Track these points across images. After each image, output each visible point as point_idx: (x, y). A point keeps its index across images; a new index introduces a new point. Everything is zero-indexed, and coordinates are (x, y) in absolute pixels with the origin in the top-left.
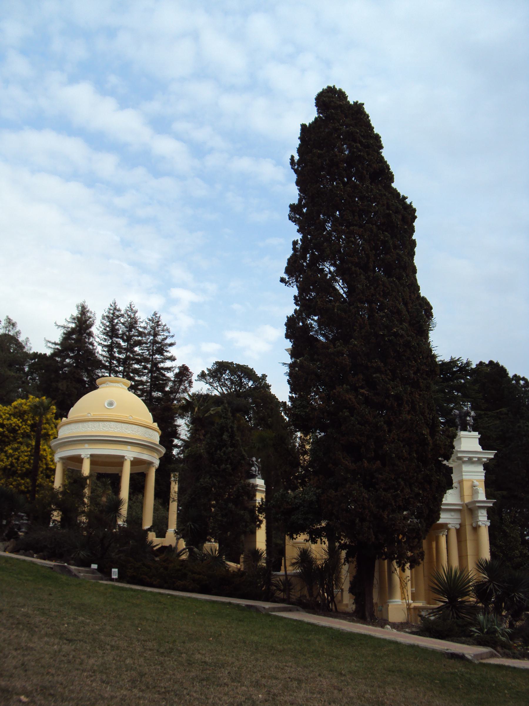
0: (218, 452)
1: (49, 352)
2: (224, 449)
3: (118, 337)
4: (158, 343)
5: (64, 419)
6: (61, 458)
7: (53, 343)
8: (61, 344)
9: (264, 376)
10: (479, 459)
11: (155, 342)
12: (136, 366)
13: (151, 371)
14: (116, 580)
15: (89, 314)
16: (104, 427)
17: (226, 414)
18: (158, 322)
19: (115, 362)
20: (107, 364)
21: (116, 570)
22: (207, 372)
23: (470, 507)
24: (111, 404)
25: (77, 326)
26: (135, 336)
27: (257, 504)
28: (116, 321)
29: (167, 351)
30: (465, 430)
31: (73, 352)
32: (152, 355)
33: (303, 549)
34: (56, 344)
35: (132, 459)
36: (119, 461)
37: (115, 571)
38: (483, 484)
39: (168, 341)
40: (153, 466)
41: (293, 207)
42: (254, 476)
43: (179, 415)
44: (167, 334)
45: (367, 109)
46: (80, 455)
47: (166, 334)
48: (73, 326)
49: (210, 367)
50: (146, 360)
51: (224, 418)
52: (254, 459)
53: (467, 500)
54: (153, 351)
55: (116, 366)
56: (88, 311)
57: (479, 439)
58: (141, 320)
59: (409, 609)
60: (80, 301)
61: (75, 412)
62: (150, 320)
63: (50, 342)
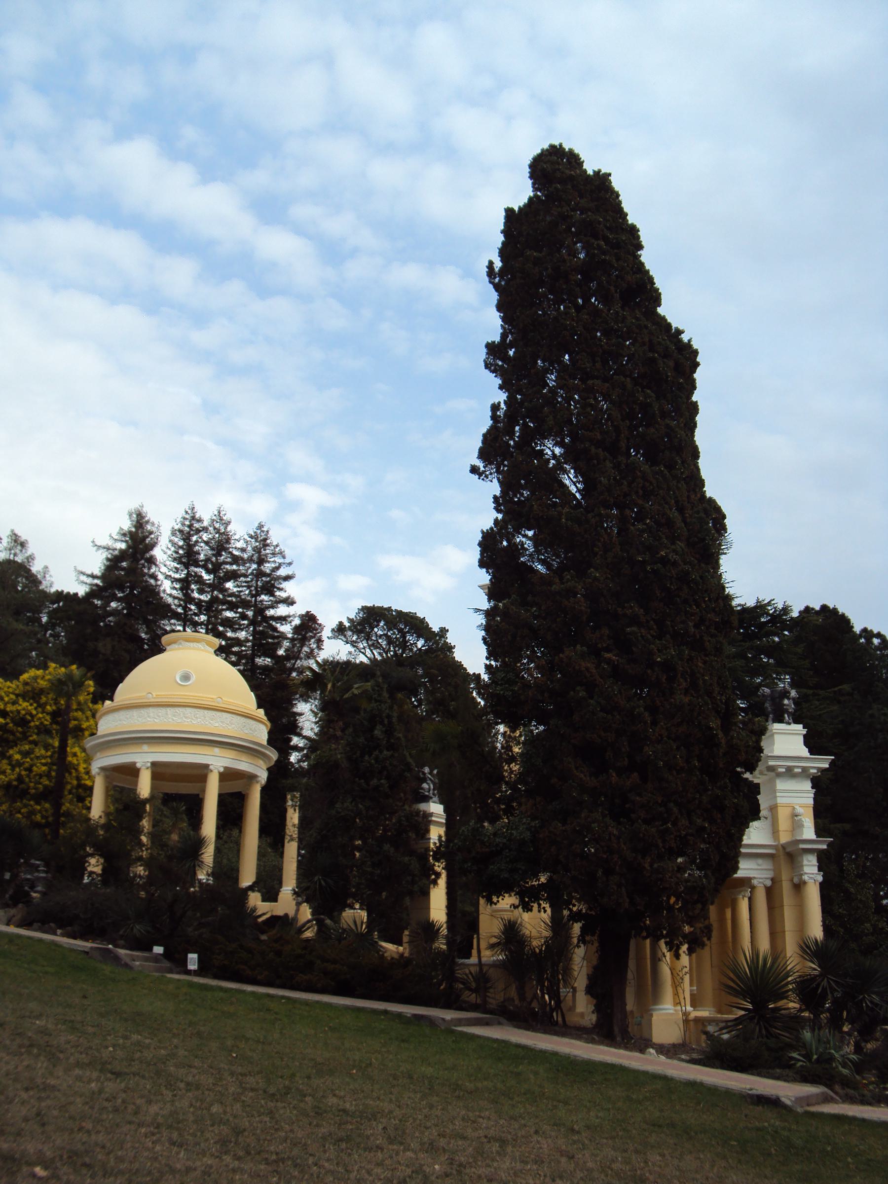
0: (367, 758)
1: (81, 591)
2: (377, 752)
3: (198, 566)
4: (265, 574)
5: (108, 703)
6: (103, 769)
7: (88, 576)
8: (103, 577)
9: (443, 631)
10: (805, 769)
11: (260, 574)
12: (229, 614)
13: (253, 622)
14: (195, 973)
15: (149, 527)
16: (174, 716)
17: (380, 695)
18: (265, 540)
19: (193, 607)
20: (180, 610)
21: (195, 956)
22: (347, 624)
23: (788, 850)
24: (186, 677)
25: (129, 547)
26: (227, 563)
27: (432, 846)
28: (194, 538)
29: (280, 589)
30: (780, 720)
31: (122, 590)
32: (255, 596)
33: (509, 921)
34: (93, 576)
35: (222, 770)
36: (200, 773)
37: (193, 957)
38: (811, 812)
39: (282, 572)
40: (257, 782)
41: (491, 348)
42: (426, 799)
43: (301, 696)
44: (281, 561)
45: (616, 183)
46: (135, 763)
47: (279, 560)
48: (123, 546)
49: (352, 616)
50: (246, 604)
51: (376, 701)
52: (427, 770)
53: (784, 839)
54: (256, 588)
55: (195, 614)
56: (147, 522)
57: (805, 736)
58: (237, 537)
59: (686, 1021)
60: (134, 505)
61: (125, 691)
62: (251, 537)
63: (84, 574)
